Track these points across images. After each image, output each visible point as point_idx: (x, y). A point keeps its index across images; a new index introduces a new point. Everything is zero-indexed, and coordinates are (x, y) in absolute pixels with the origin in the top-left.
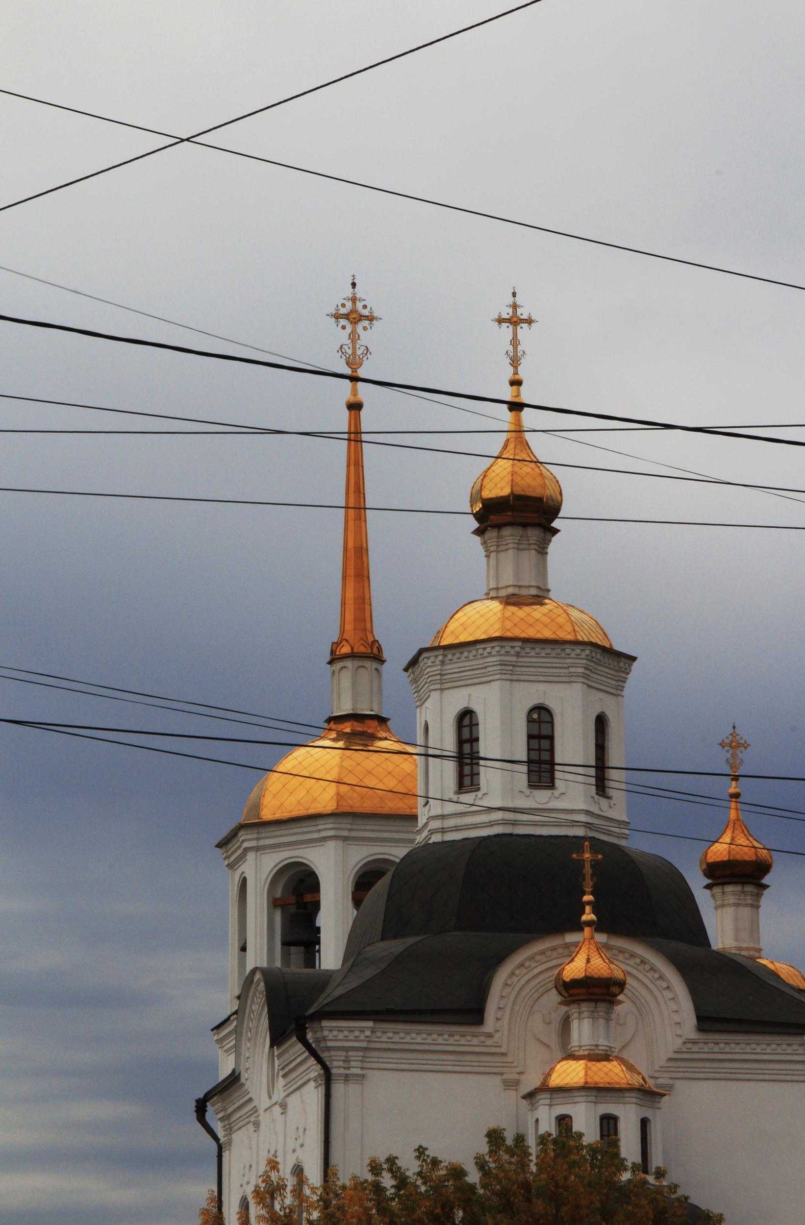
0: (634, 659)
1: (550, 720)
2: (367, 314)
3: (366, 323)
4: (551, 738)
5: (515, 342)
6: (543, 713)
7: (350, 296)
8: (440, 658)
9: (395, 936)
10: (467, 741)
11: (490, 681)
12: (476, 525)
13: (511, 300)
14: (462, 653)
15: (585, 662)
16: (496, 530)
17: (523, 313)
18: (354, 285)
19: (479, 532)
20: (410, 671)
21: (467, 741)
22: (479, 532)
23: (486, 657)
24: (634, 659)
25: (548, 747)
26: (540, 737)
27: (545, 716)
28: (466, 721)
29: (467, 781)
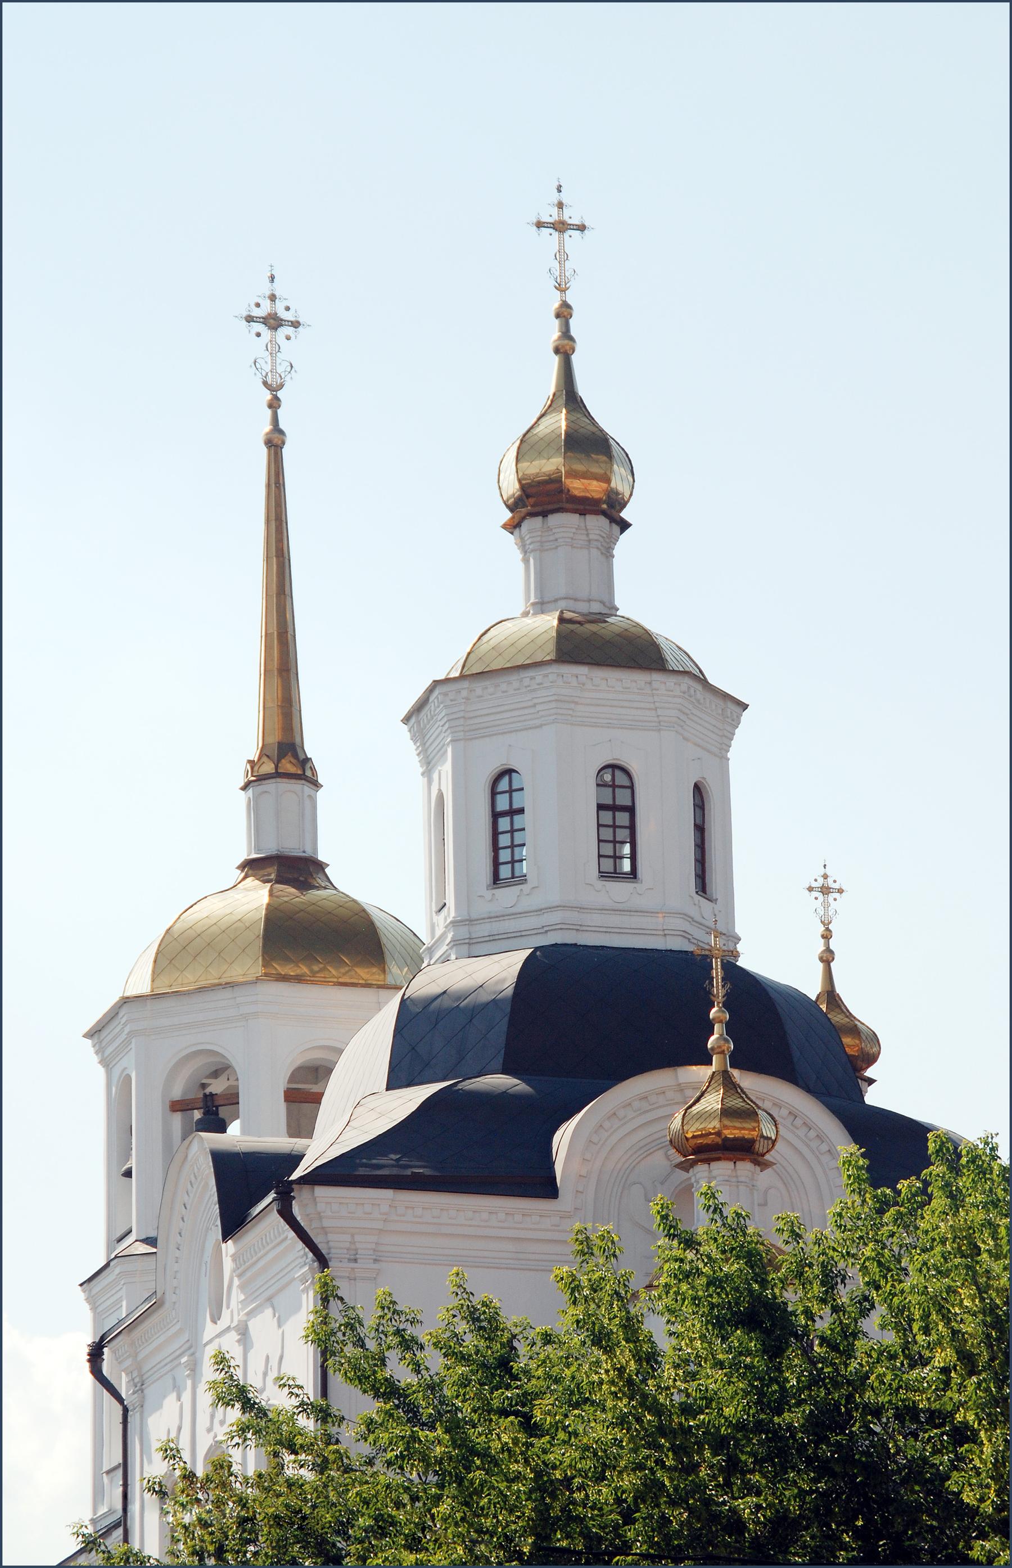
0: (745, 707)
1: (627, 783)
2: (293, 319)
3: (288, 330)
4: (631, 810)
5: (562, 256)
6: (618, 773)
7: (268, 293)
8: (464, 693)
9: (411, 1083)
10: (503, 814)
11: (541, 726)
12: (508, 515)
13: (555, 197)
14: (497, 686)
15: (679, 700)
16: (541, 518)
17: (572, 216)
18: (272, 278)
19: (513, 526)
20: (413, 720)
21: (503, 814)
22: (513, 526)
23: (534, 690)
24: (745, 707)
25: (627, 823)
26: (614, 808)
27: (621, 779)
28: (504, 785)
29: (505, 871)
